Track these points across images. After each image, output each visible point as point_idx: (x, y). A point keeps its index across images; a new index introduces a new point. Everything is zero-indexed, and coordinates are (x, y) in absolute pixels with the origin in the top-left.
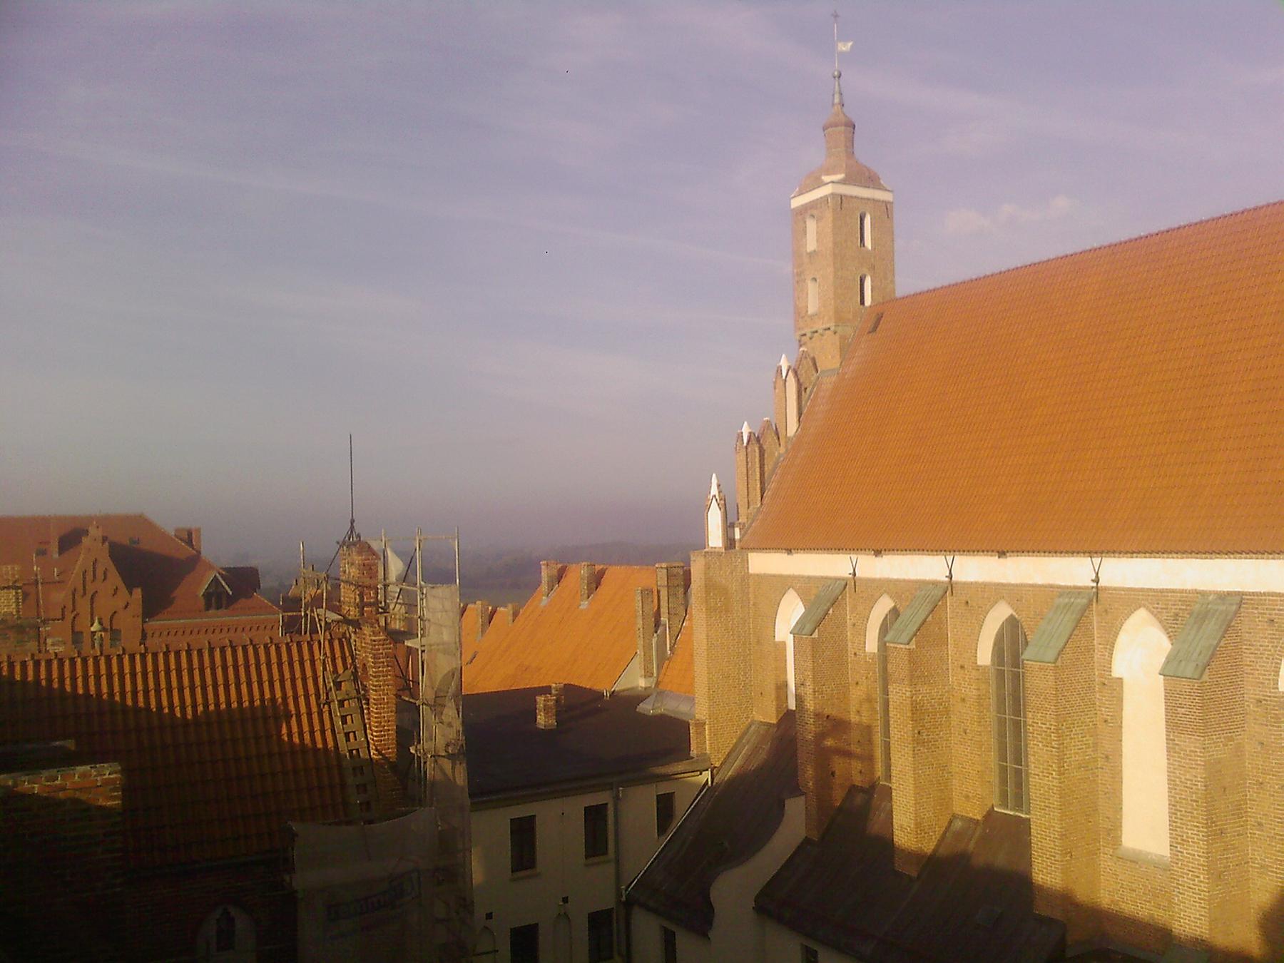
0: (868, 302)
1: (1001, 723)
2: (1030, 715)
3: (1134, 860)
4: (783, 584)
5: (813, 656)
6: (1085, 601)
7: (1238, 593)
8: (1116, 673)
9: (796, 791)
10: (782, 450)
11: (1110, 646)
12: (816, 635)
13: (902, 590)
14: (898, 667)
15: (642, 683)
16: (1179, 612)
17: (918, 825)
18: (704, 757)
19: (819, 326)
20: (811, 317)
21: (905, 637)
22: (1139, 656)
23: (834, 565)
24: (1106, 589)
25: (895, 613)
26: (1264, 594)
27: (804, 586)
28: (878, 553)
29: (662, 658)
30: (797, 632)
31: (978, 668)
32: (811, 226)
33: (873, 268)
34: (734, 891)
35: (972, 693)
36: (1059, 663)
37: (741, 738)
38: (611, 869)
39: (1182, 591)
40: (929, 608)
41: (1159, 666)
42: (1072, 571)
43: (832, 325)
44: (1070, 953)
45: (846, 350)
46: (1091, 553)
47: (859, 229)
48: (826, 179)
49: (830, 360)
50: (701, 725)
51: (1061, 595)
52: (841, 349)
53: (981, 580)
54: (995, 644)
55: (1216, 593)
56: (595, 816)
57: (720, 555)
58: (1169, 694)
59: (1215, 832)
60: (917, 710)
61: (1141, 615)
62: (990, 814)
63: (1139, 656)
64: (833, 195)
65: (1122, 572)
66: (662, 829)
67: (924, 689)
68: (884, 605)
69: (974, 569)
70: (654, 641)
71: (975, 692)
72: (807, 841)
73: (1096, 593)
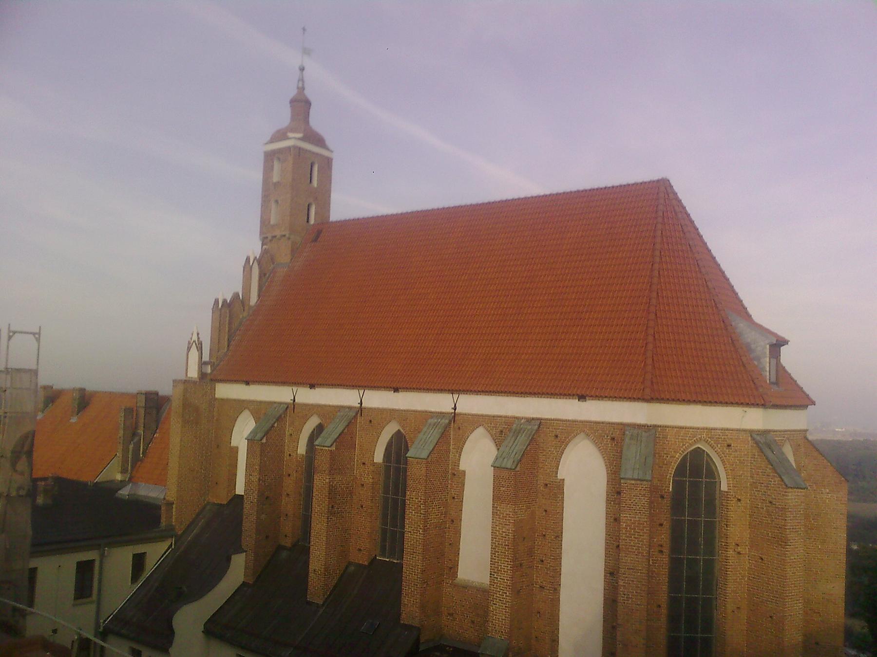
0: (312, 222)
1: (386, 500)
2: (408, 493)
3: (465, 587)
4: (240, 405)
5: (261, 455)
6: (447, 421)
7: (538, 419)
8: (462, 467)
9: (239, 550)
10: (245, 314)
11: (459, 450)
12: (264, 441)
13: (328, 412)
14: (322, 462)
15: (119, 477)
16: (502, 429)
17: (326, 570)
18: (170, 529)
19: (278, 233)
20: (273, 226)
21: (328, 443)
22: (478, 458)
23: (281, 394)
24: (460, 414)
25: (320, 429)
26: (554, 420)
27: (258, 409)
28: (312, 386)
29: (136, 460)
30: (250, 440)
31: (374, 464)
32: (277, 165)
33: (316, 199)
34: (190, 620)
35: (368, 480)
36: (429, 459)
37: (198, 515)
38: (93, 607)
39: (506, 417)
40: (346, 424)
41: (491, 462)
42: (440, 403)
43: (287, 234)
44: (422, 648)
45: (295, 251)
46: (452, 392)
47: (301, 167)
48: (290, 135)
49: (284, 256)
50: (170, 504)
51: (432, 418)
52: (292, 251)
53: (381, 407)
54: (386, 449)
55: (525, 418)
56: (85, 569)
57: (195, 383)
58: (496, 478)
59: (517, 566)
60: (332, 492)
61: (480, 431)
62: (374, 560)
63: (478, 458)
64: (295, 147)
65: (472, 404)
66: (135, 578)
67: (338, 478)
68: (313, 423)
69: (377, 399)
70: (131, 447)
71: (371, 480)
72: (244, 584)
73: (454, 416)
